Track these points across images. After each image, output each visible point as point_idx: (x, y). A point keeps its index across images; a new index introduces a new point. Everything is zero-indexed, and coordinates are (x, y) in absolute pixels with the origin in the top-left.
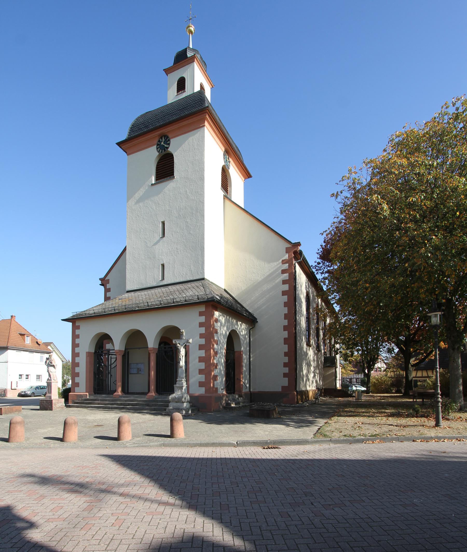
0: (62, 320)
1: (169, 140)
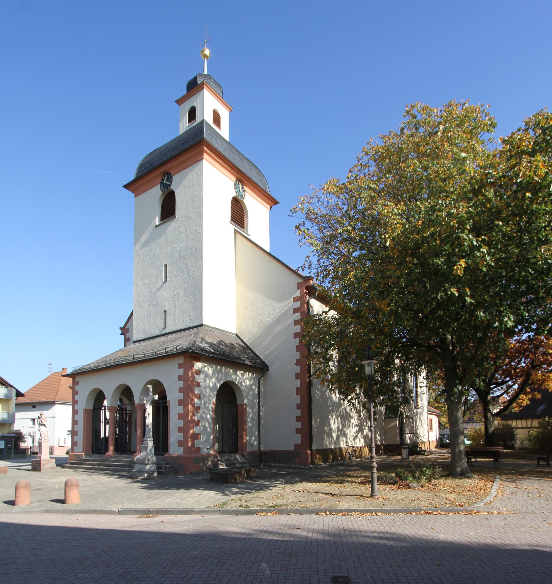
1: (171, 178)
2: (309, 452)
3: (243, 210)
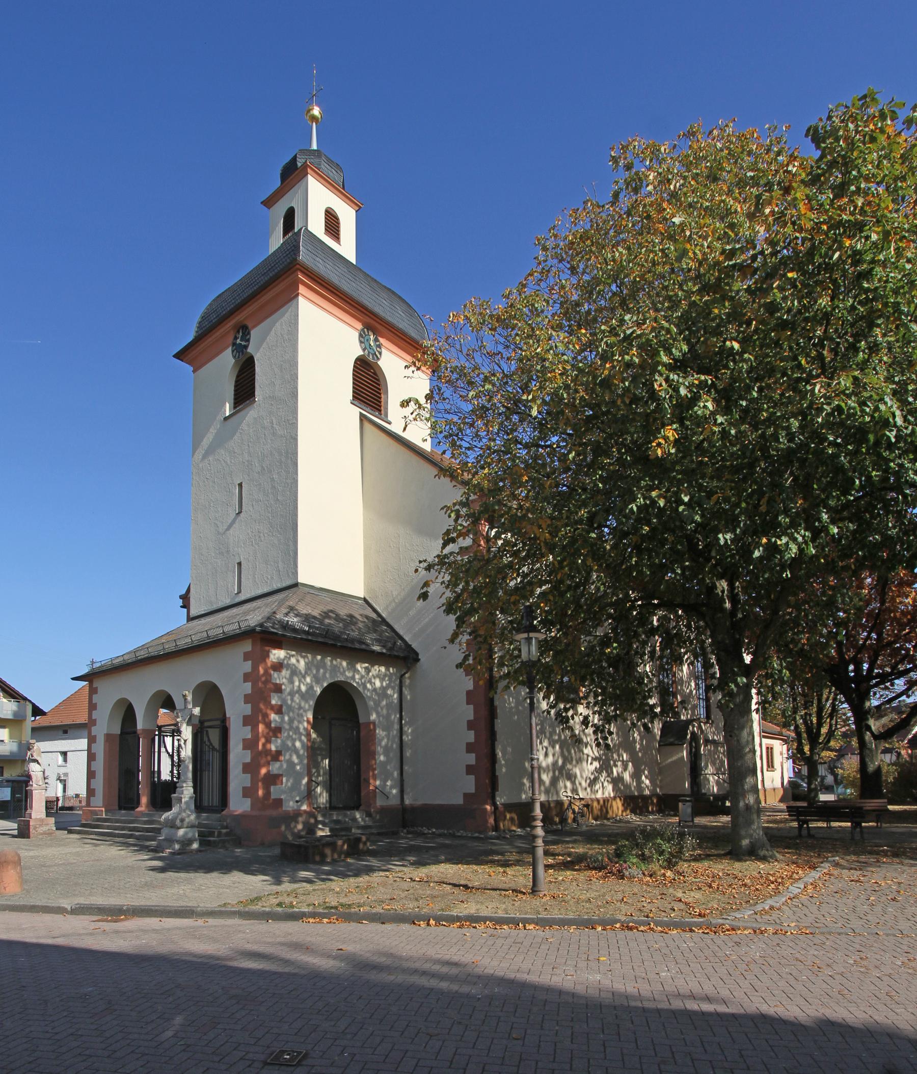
0: (73, 679)
1: (249, 333)
2: (488, 807)
3: (378, 380)
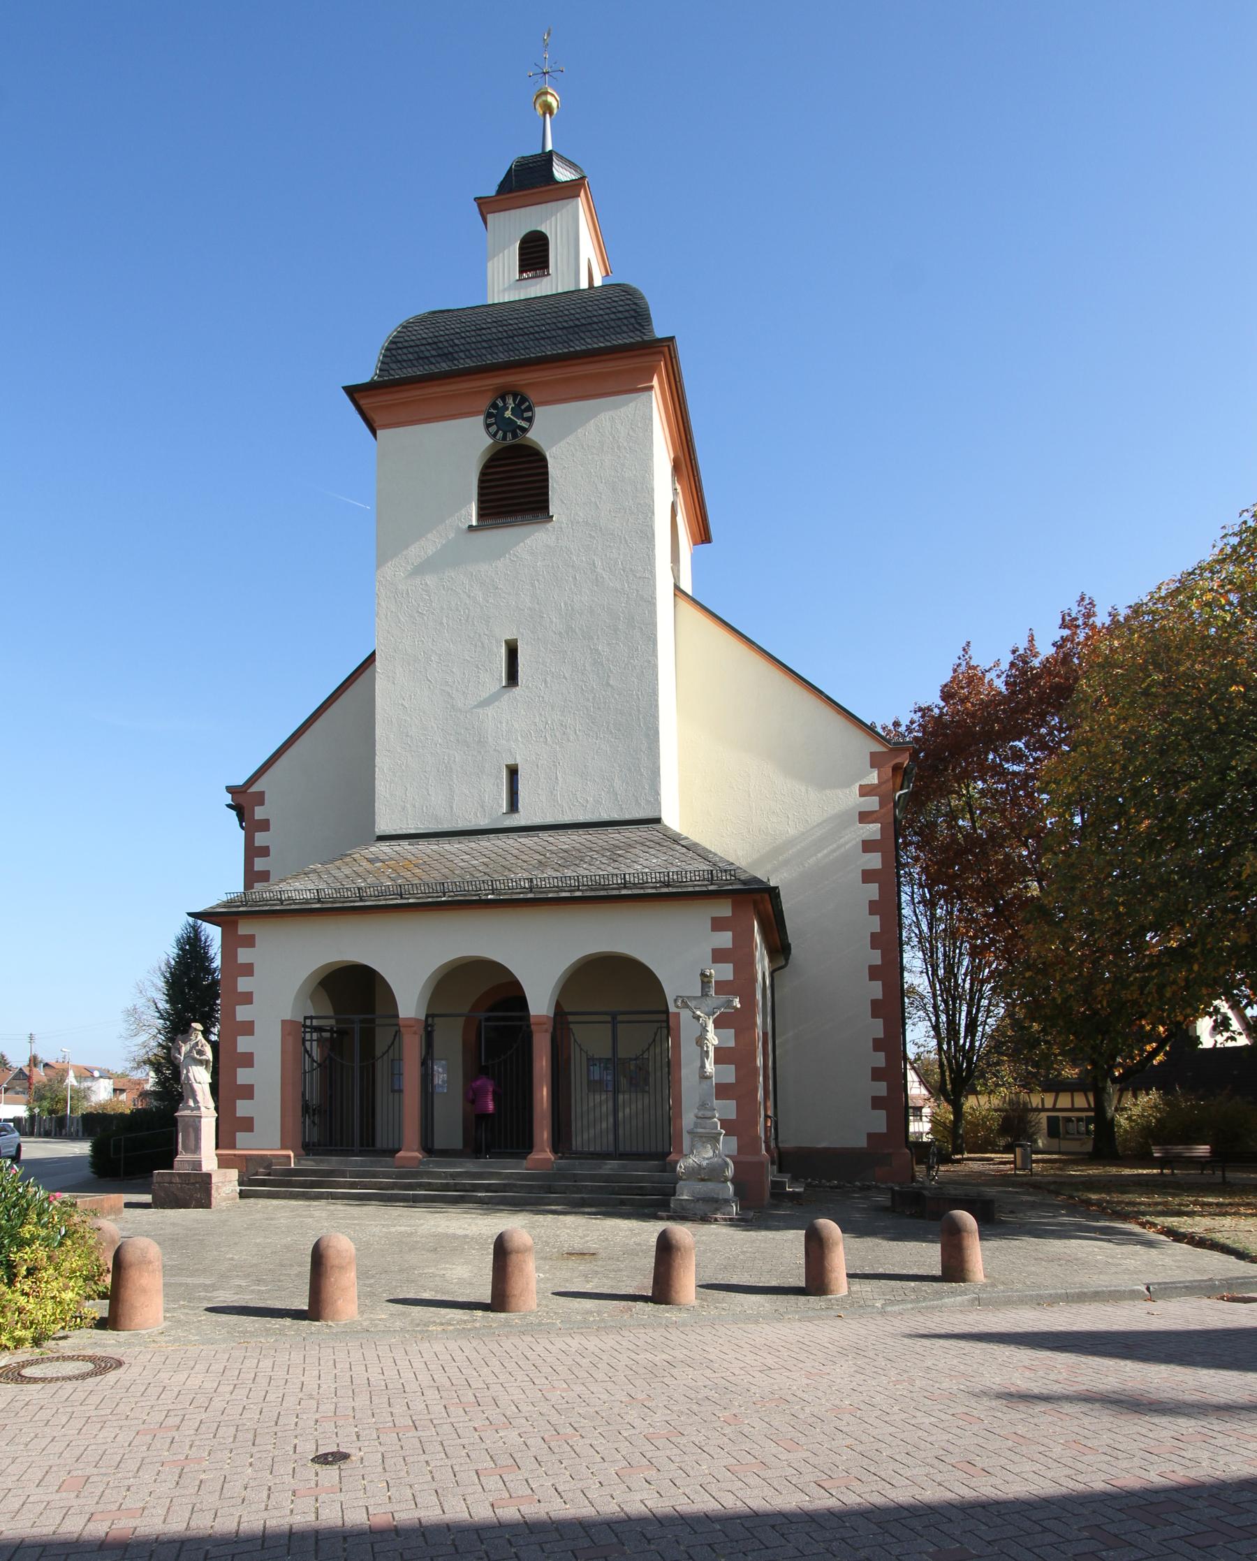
1: (529, 409)
